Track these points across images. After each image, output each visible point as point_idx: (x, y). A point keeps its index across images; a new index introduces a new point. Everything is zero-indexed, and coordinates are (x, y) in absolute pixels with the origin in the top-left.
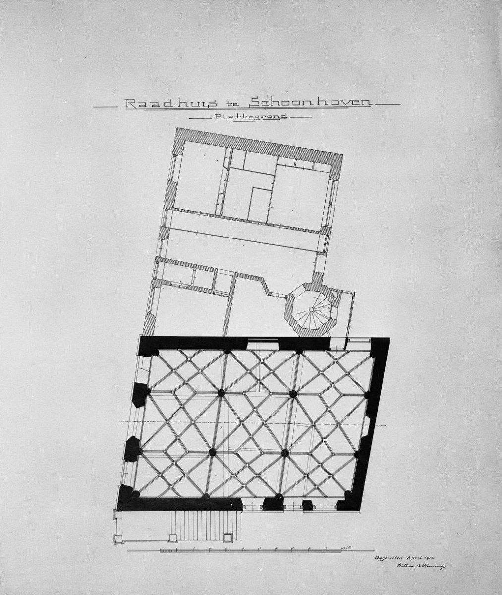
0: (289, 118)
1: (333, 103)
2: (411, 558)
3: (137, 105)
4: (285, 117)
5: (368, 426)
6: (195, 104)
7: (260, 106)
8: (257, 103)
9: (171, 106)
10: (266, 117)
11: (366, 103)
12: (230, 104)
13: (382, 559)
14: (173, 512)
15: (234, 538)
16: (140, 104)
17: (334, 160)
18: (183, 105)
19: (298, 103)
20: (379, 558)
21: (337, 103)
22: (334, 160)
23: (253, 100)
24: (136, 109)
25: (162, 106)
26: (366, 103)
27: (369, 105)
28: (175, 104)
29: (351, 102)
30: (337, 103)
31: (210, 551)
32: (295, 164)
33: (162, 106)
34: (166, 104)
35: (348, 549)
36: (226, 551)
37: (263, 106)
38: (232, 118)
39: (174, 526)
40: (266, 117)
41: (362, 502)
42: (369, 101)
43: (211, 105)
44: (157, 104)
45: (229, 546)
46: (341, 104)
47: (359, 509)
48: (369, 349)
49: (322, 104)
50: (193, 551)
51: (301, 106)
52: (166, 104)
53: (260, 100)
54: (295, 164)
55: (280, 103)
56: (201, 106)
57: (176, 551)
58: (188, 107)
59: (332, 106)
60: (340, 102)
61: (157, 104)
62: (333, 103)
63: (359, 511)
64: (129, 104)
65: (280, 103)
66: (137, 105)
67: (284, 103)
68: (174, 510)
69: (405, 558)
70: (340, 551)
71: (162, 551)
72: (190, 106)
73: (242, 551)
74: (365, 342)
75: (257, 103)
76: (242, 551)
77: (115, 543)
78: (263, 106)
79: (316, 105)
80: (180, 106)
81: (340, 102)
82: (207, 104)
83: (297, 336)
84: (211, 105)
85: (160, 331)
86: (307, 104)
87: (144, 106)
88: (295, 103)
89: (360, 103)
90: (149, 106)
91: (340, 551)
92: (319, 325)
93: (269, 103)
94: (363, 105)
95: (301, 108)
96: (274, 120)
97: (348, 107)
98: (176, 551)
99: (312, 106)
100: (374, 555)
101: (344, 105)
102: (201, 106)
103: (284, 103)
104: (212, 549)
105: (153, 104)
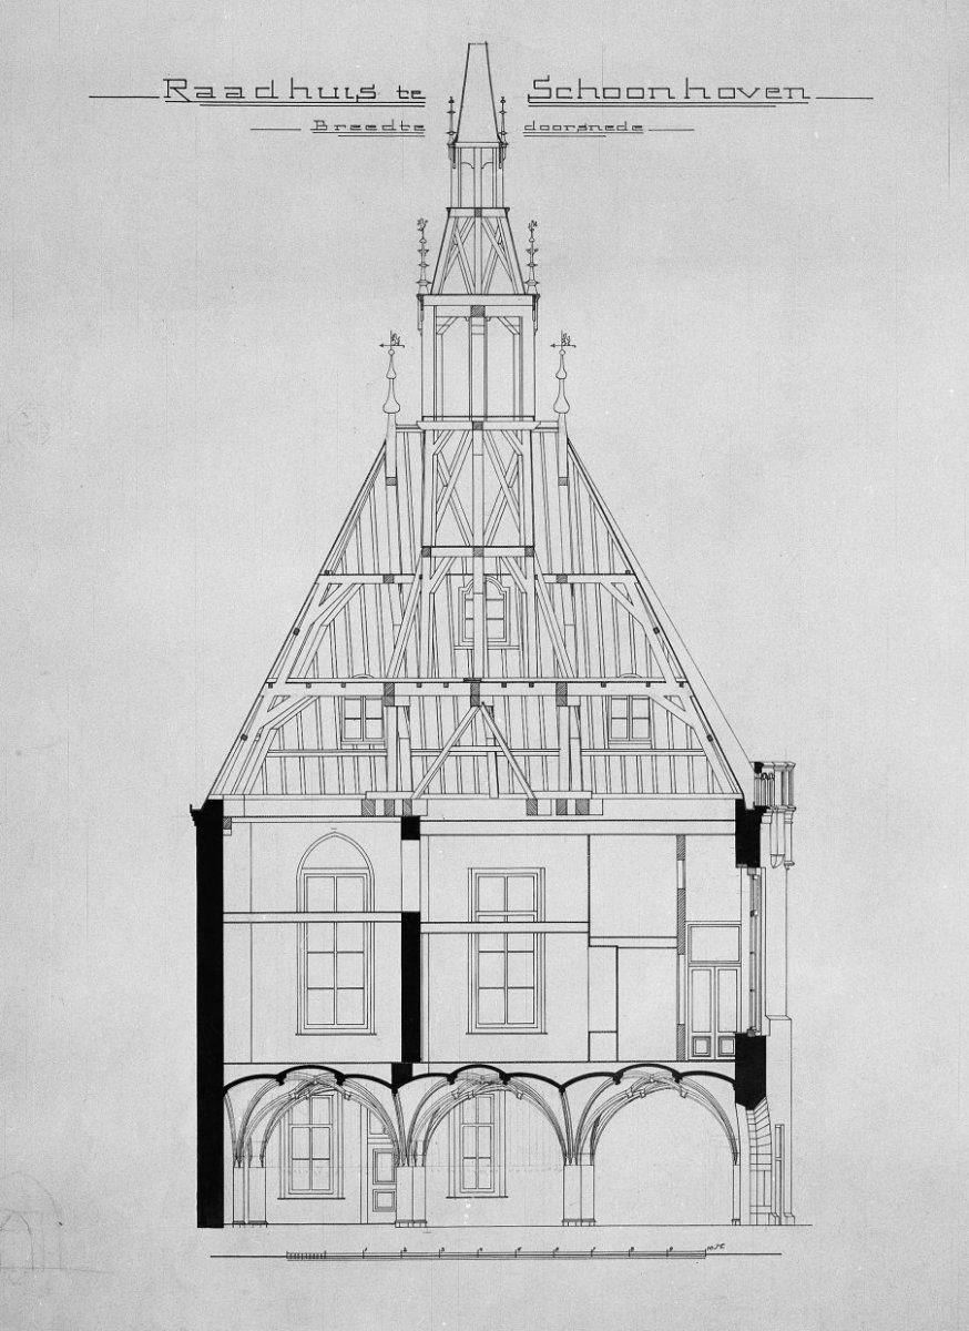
1: (260, 93)
3: (190, 93)
8: (546, 93)
9: (272, 97)
11: (797, 95)
16: (227, 91)
18: (300, 96)
21: (730, 93)
24: (189, 101)
26: (797, 95)
28: (283, 93)
34: (560, 91)
37: (768, 100)
39: (452, 1185)
41: (734, 851)
42: (307, 89)
43: (365, 95)
46: (740, 97)
48: (225, 916)
49: (696, 96)
51: (647, 99)
53: (553, 84)
55: (600, 94)
61: (238, 91)
62: (260, 93)
64: (172, 92)
65: (600, 94)
66: (190, 93)
67: (608, 93)
71: (290, 1257)
75: (546, 93)
79: (680, 98)
82: (354, 92)
84: (365, 95)
86: (661, 96)
88: (632, 93)
90: (220, 95)
93: (575, 93)
94: (790, 100)
95: (647, 105)
103: (608, 93)
104: (447, 1250)
105: (199, 91)
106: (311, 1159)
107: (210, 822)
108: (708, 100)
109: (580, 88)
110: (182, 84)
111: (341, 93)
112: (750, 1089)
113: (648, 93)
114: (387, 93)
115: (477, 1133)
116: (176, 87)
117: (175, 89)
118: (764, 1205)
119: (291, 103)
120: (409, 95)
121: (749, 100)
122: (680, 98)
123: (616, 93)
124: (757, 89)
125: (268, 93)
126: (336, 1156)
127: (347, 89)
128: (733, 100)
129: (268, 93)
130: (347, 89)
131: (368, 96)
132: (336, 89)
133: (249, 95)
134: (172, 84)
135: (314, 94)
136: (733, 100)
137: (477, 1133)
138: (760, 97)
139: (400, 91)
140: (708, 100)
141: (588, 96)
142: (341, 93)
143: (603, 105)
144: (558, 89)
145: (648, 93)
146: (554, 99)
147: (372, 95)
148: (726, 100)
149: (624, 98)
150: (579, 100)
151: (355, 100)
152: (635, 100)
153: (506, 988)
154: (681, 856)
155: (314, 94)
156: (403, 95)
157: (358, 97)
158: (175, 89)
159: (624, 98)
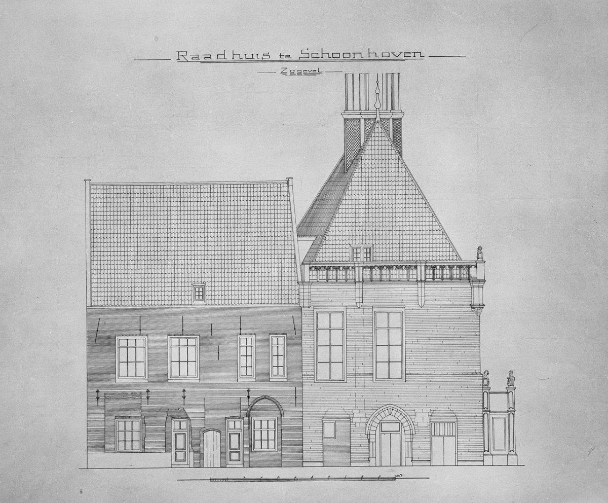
0: (324, 73)
4: (314, 73)
6: (249, 56)
7: (341, 58)
11: (418, 56)
19: (348, 55)
21: (387, 55)
23: (303, 52)
26: (418, 56)
27: (421, 58)
32: (124, 347)
33: (202, 59)
37: (313, 59)
42: (226, 418)
46: (392, 57)
52: (219, 57)
53: (310, 52)
54: (124, 347)
55: (331, 56)
56: (256, 59)
58: (363, 58)
59: (205, 60)
60: (391, 55)
64: (181, 58)
65: (331, 56)
67: (345, 55)
72: (244, 59)
74: (509, 402)
78: (313, 59)
81: (391, 55)
82: (260, 56)
87: (196, 58)
89: (412, 55)
93: (320, 55)
104: (381, 477)
106: (246, 356)
108: (241, 60)
115: (330, 375)
116: (181, 55)
118: (373, 442)
121: (398, 58)
122: (366, 57)
124: (401, 53)
125: (223, 57)
126: (459, 367)
127: (257, 54)
128: (269, 59)
129: (223, 57)
130: (257, 54)
133: (214, 58)
135: (243, 57)
137: (330, 375)
138: (402, 57)
139: (280, 55)
140: (241, 60)
141: (326, 57)
142: (255, 56)
143: (332, 61)
144: (421, 56)
145: (352, 55)
146: (310, 58)
149: (341, 58)
150: (322, 59)
155: (243, 57)
156: (282, 57)
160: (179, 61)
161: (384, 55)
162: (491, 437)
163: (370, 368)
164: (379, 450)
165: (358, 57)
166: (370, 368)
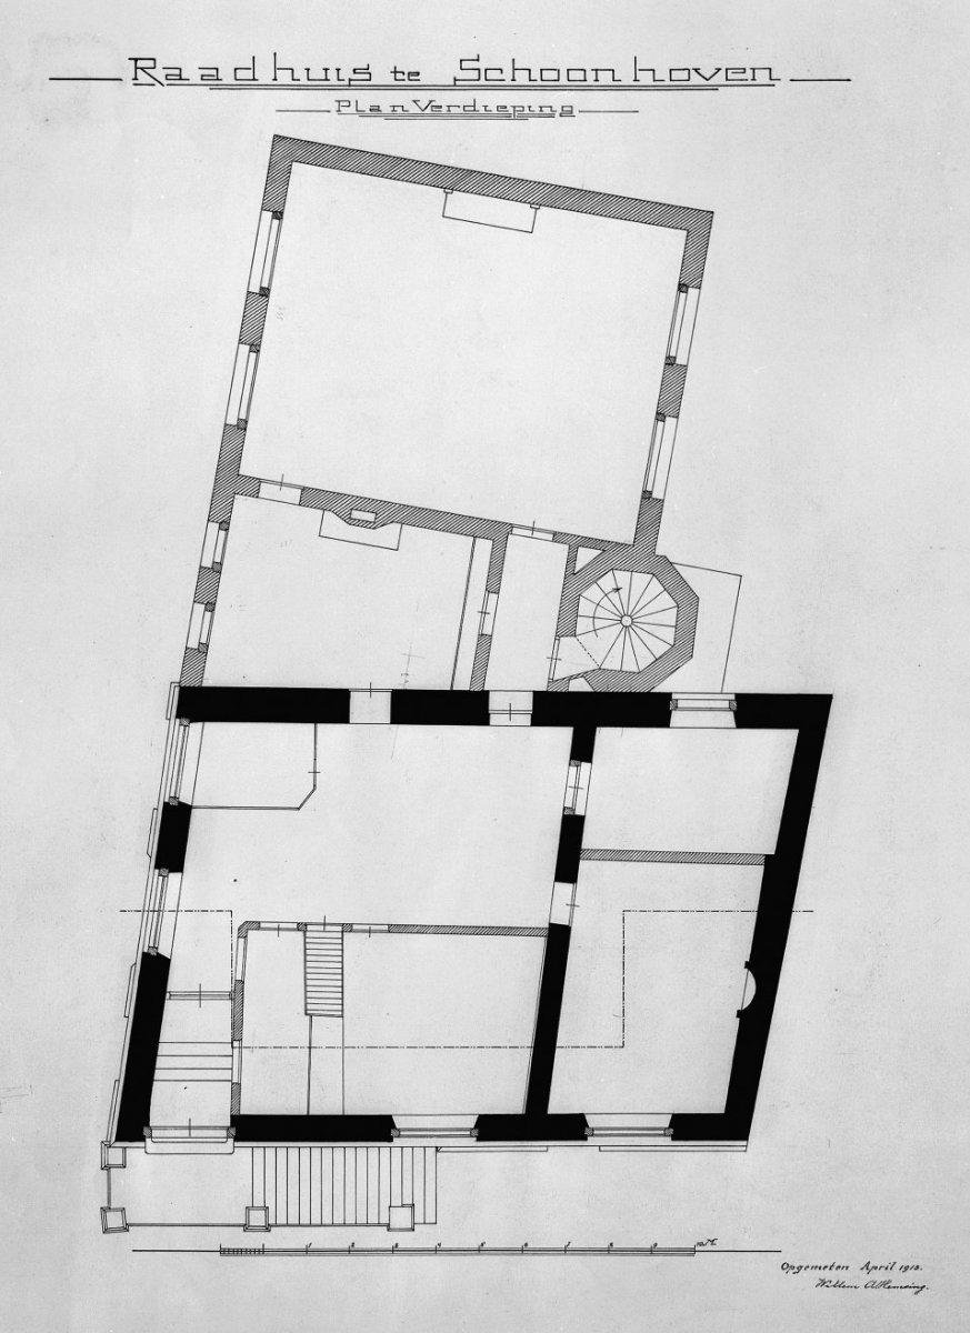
2: (870, 1267)
4: (567, 112)
5: (753, 916)
6: (317, 73)
8: (474, 75)
9: (254, 79)
10: (461, 110)
11: (762, 77)
12: (399, 76)
13: (796, 1270)
14: (158, 1074)
15: (419, 1219)
17: (696, 224)
20: (786, 1267)
22: (696, 224)
23: (465, 65)
25: (227, 78)
26: (762, 77)
29: (722, 73)
30: (684, 75)
31: (350, 1251)
35: (709, 1247)
36: (395, 1250)
37: (309, 83)
38: (375, 110)
40: (461, 110)
42: (236, 69)
44: (177, 72)
45: (405, 1240)
46: (696, 80)
47: (746, 1138)
50: (307, 1251)
51: (590, 81)
53: (482, 65)
56: (333, 81)
57: (262, 1251)
61: (177, 72)
63: (744, 1143)
66: (159, 74)
68: (155, 1061)
69: (855, 1266)
70: (692, 1252)
71: (223, 1252)
72: (304, 81)
73: (436, 1251)
76: (436, 1251)
77: (106, 1230)
80: (597, 80)
82: (346, 74)
83: (590, 690)
85: (218, 674)
87: (211, 78)
91: (692, 1252)
92: (645, 660)
93: (507, 75)
94: (754, 82)
95: (590, 88)
96: (523, 117)
97: (715, 88)
98: (262, 1251)
99: (616, 83)
100: (778, 1259)
101: (704, 82)
102: (333, 81)
107: (849, 80)
109: (514, 69)
110: (151, 63)
111: (332, 75)
112: (572, 827)
113: (591, 76)
114: (382, 75)
117: (142, 69)
119: (637, 87)
120: (406, 77)
121: (706, 83)
123: (554, 75)
127: (338, 70)
130: (338, 70)
131: (362, 78)
132: (326, 70)
134: (140, 64)
135: (300, 74)
136: (556, 83)
142: (332, 75)
144: (486, 70)
145: (591, 76)
146: (483, 82)
147: (367, 76)
148: (318, 83)
149: (563, 81)
151: (346, 82)
152: (318, 83)
153: (344, 1048)
154: (650, 504)
157: (350, 80)
158: (142, 69)
159: (563, 81)
160: (136, 82)
161: (675, 75)
162: (735, 1148)
163: (313, 995)
164: (713, 706)
165: (605, 78)
166: (313, 995)
